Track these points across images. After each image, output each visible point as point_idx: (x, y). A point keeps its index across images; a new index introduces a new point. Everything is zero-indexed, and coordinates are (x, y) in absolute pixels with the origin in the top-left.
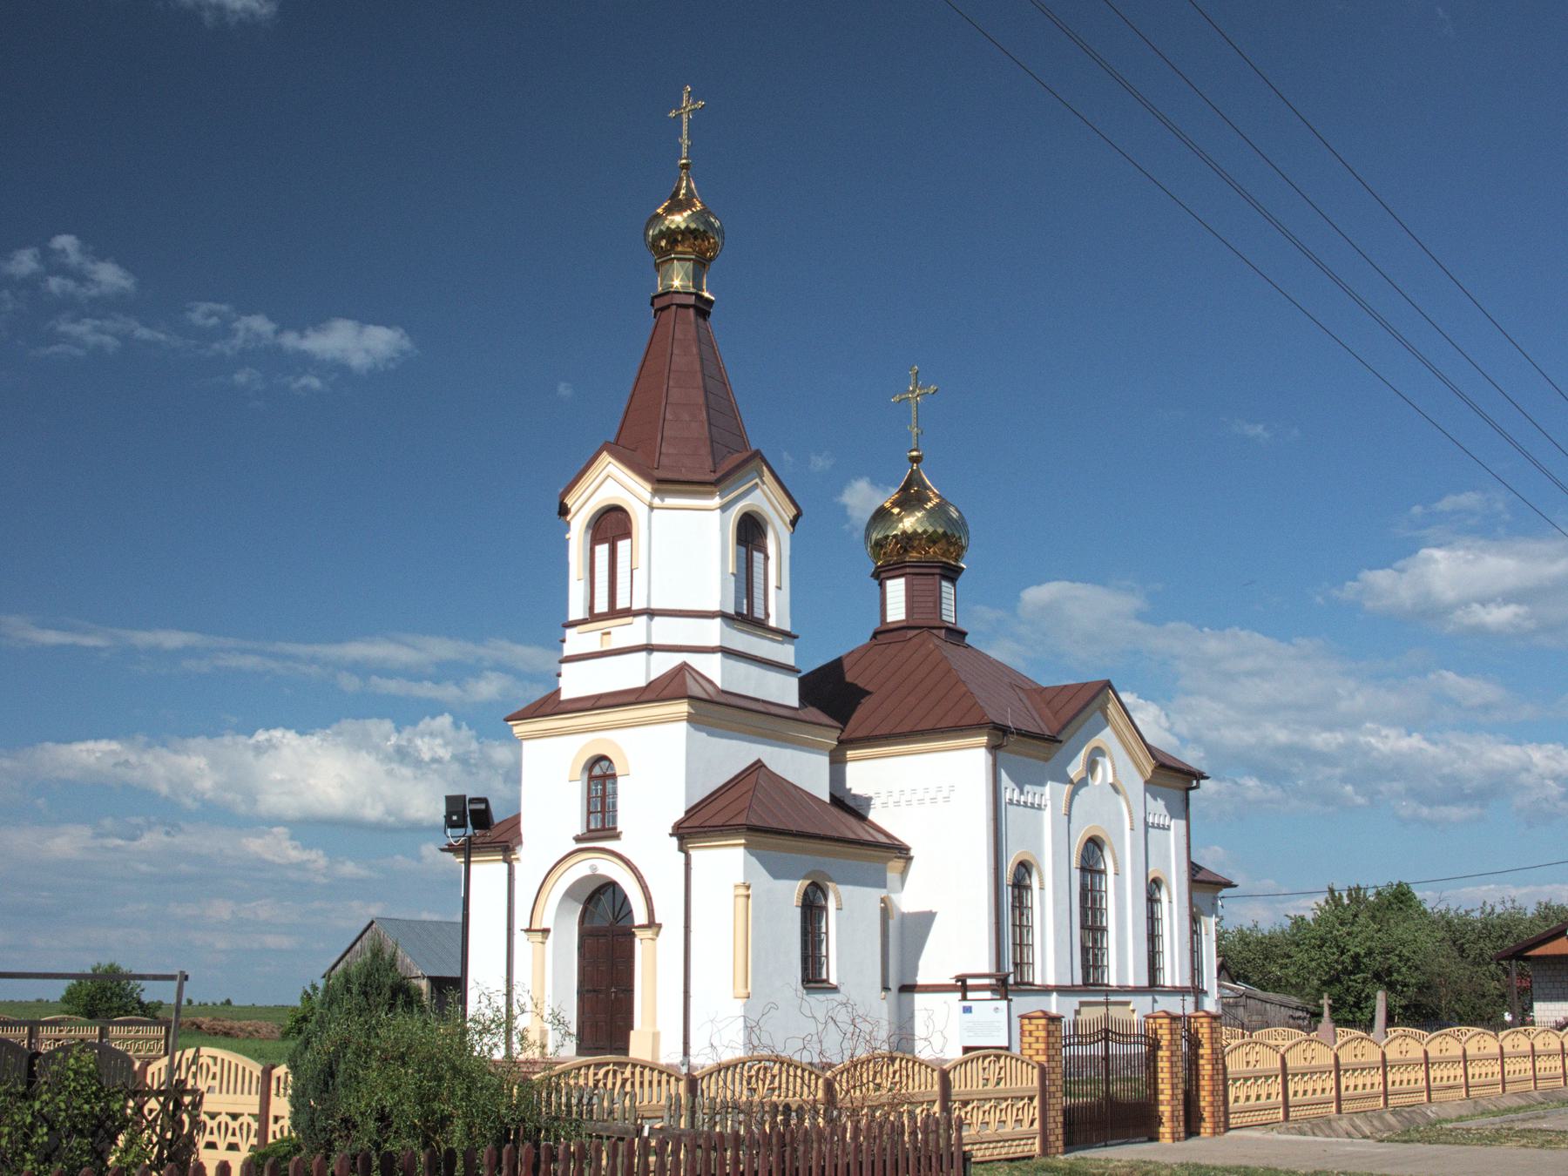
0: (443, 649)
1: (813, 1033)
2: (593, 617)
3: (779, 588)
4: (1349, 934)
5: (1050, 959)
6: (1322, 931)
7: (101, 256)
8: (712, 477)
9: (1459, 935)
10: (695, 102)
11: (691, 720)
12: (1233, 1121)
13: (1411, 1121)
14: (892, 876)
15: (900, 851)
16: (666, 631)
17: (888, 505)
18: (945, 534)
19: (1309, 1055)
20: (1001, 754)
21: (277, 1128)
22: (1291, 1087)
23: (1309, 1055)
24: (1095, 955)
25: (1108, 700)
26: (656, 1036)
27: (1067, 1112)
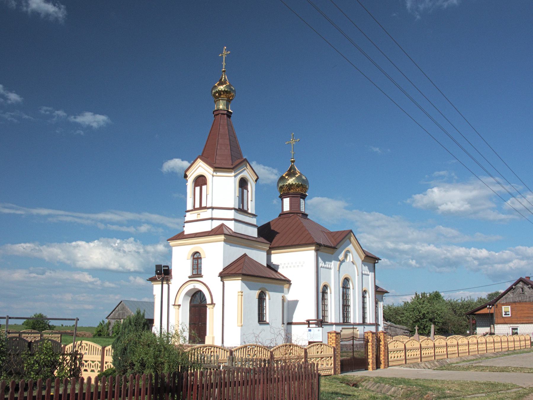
0: (130, 216)
1: (271, 336)
2: (195, 209)
3: (252, 201)
4: (422, 307)
5: (333, 314)
6: (414, 306)
7: (11, 91)
8: (232, 167)
9: (454, 307)
10: (227, 52)
11: (225, 241)
12: (390, 364)
13: (442, 364)
14: (285, 289)
15: (288, 282)
16: (217, 214)
17: (284, 175)
18: (302, 185)
19: (396, 345)
20: (319, 252)
21: (106, 365)
22: (407, 354)
23: (396, 345)
24: (347, 314)
25: (351, 236)
26: (213, 338)
27: (342, 362)
